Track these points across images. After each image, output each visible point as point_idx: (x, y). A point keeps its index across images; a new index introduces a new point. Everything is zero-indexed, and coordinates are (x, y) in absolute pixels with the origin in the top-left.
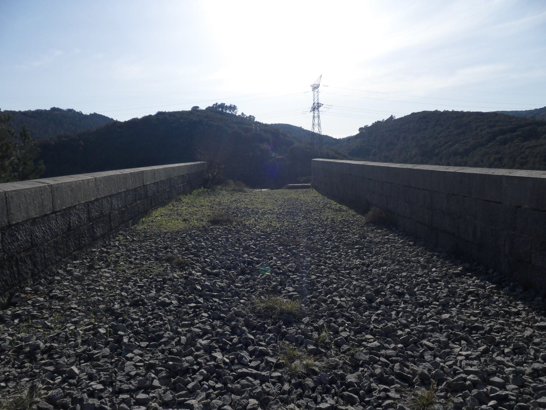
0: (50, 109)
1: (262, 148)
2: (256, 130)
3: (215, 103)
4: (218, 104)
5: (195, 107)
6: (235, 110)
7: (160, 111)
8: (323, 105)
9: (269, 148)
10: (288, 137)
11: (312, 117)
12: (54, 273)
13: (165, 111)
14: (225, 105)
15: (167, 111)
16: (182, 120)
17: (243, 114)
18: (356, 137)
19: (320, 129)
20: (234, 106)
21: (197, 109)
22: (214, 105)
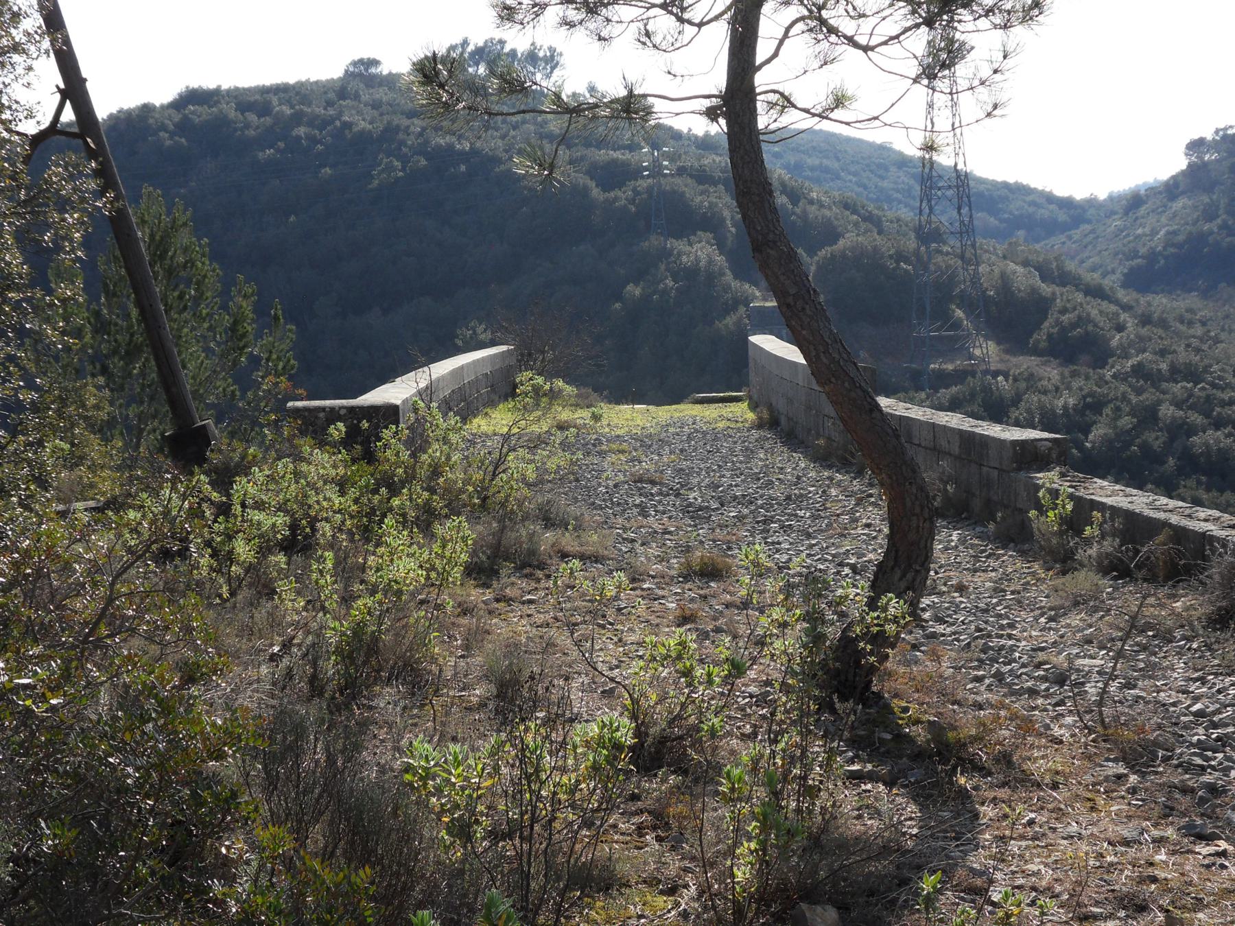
0: (158, 105)
1: (684, 259)
2: (656, 170)
3: (457, 40)
4: (471, 48)
5: (361, 62)
6: (556, 72)
7: (195, 84)
8: (973, 48)
9: (720, 259)
10: (811, 202)
11: (925, 106)
12: (148, 611)
13: (219, 86)
14: (507, 49)
15: (225, 87)
16: (301, 131)
17: (592, 89)
18: (1171, 189)
19: (957, 147)
20: (552, 50)
21: (373, 70)
22: (453, 48)
